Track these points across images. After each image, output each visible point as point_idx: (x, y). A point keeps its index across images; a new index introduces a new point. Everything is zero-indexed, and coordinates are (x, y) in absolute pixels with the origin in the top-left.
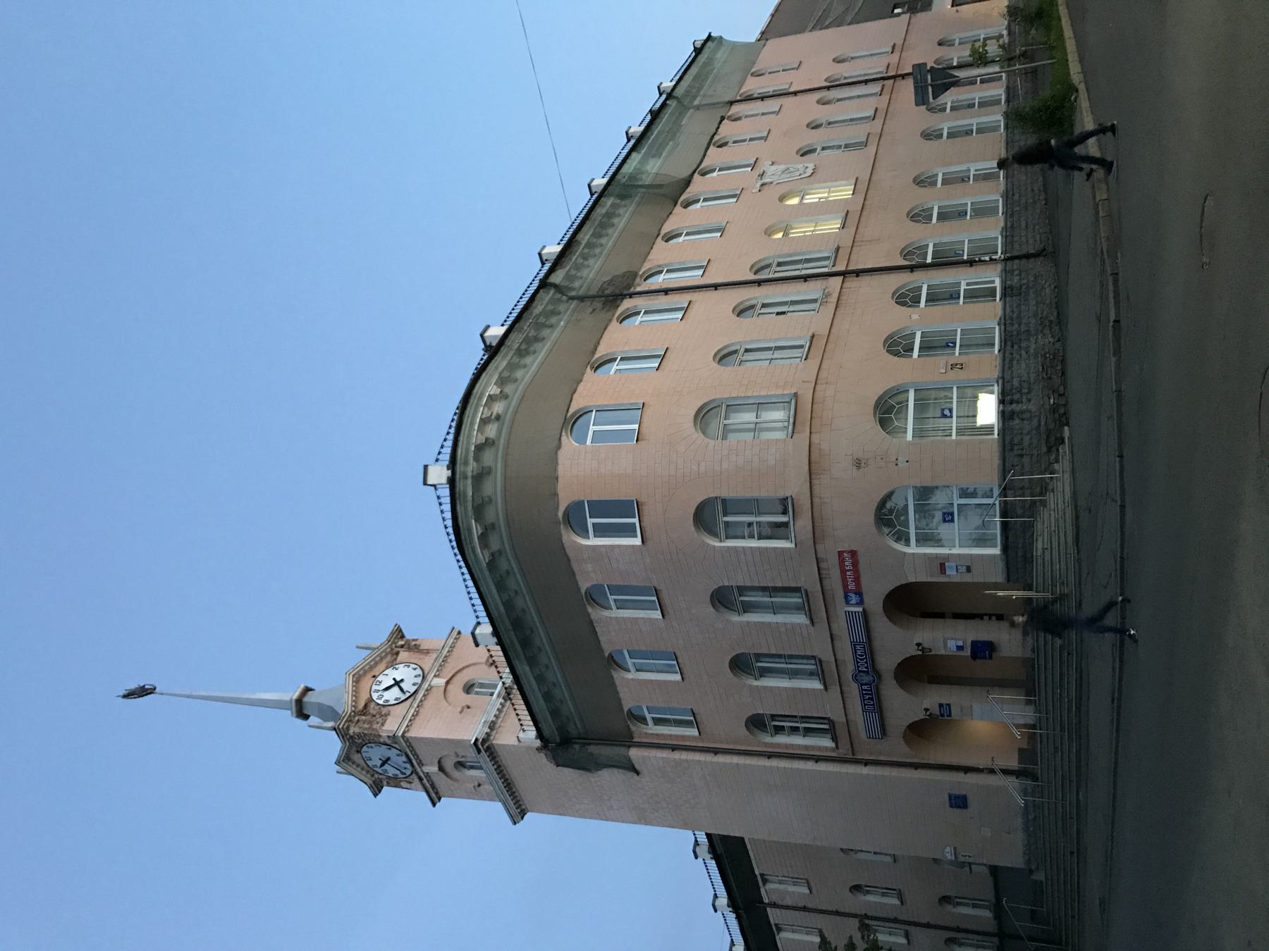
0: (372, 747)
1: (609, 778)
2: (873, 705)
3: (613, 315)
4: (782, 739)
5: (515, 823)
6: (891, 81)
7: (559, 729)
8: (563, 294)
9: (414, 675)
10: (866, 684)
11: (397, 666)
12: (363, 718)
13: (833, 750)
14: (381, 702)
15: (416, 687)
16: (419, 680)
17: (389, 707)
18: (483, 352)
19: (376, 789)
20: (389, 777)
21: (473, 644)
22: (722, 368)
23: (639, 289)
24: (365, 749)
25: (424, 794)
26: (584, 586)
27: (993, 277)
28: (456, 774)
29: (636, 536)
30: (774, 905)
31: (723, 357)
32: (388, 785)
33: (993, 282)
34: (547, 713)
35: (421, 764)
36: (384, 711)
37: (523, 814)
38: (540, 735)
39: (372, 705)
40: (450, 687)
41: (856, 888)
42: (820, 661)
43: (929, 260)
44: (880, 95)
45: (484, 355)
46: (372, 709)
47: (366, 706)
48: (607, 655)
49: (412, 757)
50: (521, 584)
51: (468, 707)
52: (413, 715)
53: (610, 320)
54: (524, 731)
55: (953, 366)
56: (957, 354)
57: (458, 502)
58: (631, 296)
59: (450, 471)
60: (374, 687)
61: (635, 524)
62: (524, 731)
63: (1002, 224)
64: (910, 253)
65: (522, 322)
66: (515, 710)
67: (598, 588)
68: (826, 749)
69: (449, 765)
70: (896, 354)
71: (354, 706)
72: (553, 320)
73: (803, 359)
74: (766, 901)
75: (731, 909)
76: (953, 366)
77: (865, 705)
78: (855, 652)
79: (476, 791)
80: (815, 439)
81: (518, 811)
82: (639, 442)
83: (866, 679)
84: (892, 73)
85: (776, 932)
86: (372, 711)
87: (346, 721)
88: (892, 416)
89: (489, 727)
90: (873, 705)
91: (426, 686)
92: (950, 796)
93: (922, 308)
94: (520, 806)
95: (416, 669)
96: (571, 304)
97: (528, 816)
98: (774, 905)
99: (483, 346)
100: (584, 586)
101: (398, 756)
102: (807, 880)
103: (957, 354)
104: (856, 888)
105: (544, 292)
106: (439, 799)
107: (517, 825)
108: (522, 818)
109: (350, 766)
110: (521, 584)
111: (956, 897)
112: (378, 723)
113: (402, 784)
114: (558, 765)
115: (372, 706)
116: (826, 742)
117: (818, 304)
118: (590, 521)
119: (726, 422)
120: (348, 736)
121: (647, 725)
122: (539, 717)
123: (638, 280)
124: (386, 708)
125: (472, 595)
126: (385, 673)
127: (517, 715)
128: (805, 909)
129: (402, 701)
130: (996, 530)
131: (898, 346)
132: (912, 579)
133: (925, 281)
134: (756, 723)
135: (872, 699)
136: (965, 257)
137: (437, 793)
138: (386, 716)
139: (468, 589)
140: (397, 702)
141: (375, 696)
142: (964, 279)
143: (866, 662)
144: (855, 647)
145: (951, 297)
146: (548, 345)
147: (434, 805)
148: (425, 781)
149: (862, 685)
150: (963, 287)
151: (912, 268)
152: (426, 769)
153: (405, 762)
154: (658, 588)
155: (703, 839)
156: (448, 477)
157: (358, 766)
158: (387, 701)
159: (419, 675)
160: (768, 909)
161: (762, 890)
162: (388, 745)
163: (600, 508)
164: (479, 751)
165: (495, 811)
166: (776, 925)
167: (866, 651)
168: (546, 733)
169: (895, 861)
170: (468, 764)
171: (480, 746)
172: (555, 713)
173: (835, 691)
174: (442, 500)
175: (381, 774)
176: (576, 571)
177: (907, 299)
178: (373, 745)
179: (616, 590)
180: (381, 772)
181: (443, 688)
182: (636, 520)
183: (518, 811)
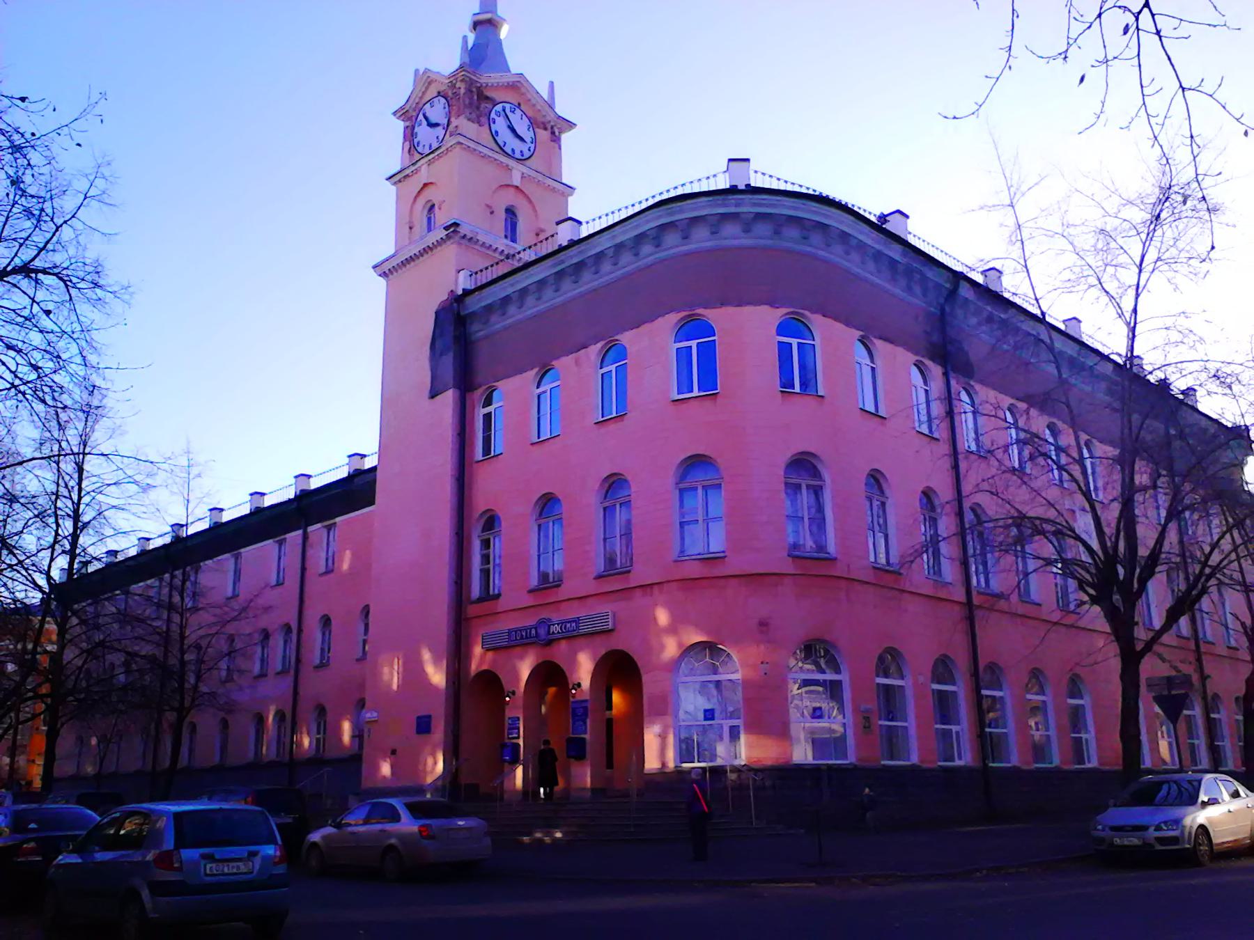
0: (445, 108)
1: (424, 376)
2: (516, 640)
3: (923, 356)
4: (476, 545)
5: (375, 267)
6: (1193, 647)
7: (473, 313)
8: (946, 300)
9: (523, 150)
10: (536, 632)
11: (531, 129)
12: (475, 97)
13: (469, 597)
14: (493, 115)
15: (510, 152)
16: (518, 155)
17: (487, 125)
18: (878, 214)
19: (402, 113)
20: (413, 127)
21: (558, 220)
22: (863, 478)
23: (953, 382)
24: (443, 100)
25: (398, 168)
26: (625, 338)
27: (965, 758)
28: (421, 201)
29: (679, 393)
30: (305, 537)
31: (876, 479)
32: (406, 128)
33: (960, 758)
34: (489, 301)
35: (430, 163)
36: (484, 120)
37: (384, 275)
38: (467, 293)
39: (489, 106)
40: (512, 190)
41: (326, 621)
42: (559, 586)
43: (984, 692)
44: (1178, 636)
45: (875, 215)
46: (485, 106)
47: (487, 98)
48: (553, 363)
49: (436, 154)
50: (626, 269)
51: (492, 213)
52: (480, 152)
53: (916, 354)
54: (471, 275)
55: (867, 719)
56: (881, 722)
57: (711, 198)
58: (946, 374)
59: (743, 188)
60: (508, 106)
61: (692, 392)
62: (471, 275)
63: (1025, 767)
64: (993, 672)
65: (912, 254)
66: (492, 266)
67: (623, 354)
68: (469, 591)
69: (429, 194)
70: (881, 659)
71: (487, 85)
72: (917, 290)
73: (875, 565)
74: (310, 529)
75: (298, 493)
76: (867, 719)
77: (516, 632)
78: (568, 622)
79: (406, 226)
80: (787, 580)
81: (386, 270)
82: (780, 393)
83: (542, 632)
84: (1203, 648)
85: (278, 539)
86: (483, 105)
87: (471, 79)
88: (707, 659)
89: (471, 238)
90: (516, 640)
91: (511, 163)
92: (429, 717)
93: (874, 680)
94: (392, 273)
95: (529, 150)
96: (935, 309)
97: (382, 282)
98: (305, 537)
99: (886, 213)
100: (625, 338)
101: (437, 137)
102: (332, 571)
103: (881, 722)
104: (326, 621)
105: (948, 277)
106: (395, 183)
107: (372, 270)
108: (380, 275)
109: (424, 84)
110: (626, 269)
111: (325, 722)
112: (470, 113)
113: (407, 143)
114: (436, 313)
115: (487, 105)
116: (476, 591)
117: (935, 578)
118: (694, 343)
119: (804, 487)
120: (454, 82)
121: (483, 407)
122: (485, 292)
123: (962, 379)
124: (487, 121)
125: (611, 216)
126: (524, 116)
127: (487, 268)
128: (303, 569)
129: (495, 139)
130: (699, 762)
131: (889, 660)
132: (645, 678)
133: (960, 689)
134: (491, 522)
135: (522, 637)
136: (988, 730)
137: (400, 181)
138: (478, 123)
139: (617, 212)
140: (494, 133)
141: (499, 108)
142: (963, 728)
143: (558, 632)
144: (573, 621)
145: (889, 712)
146: (888, 286)
147: (387, 179)
148: (413, 168)
149: (536, 628)
150: (954, 728)
151: (975, 674)
152: (424, 169)
153: (430, 146)
154: (626, 417)
155: (369, 463)
156: (736, 186)
157: (424, 93)
158: (494, 123)
159: (523, 155)
160: (300, 532)
161: (319, 525)
162: (448, 126)
163: (707, 352)
164: (446, 228)
165: (385, 247)
166: (285, 539)
167: (574, 634)
168: (468, 300)
169: (358, 660)
170: (432, 215)
171: (452, 230)
172: (489, 309)
173: (529, 601)
174: (712, 180)
175: (416, 119)
176: (640, 329)
177: (942, 669)
178: (447, 109)
179: (621, 370)
180: (418, 120)
181: (511, 184)
182: (696, 393)
183: (386, 270)
